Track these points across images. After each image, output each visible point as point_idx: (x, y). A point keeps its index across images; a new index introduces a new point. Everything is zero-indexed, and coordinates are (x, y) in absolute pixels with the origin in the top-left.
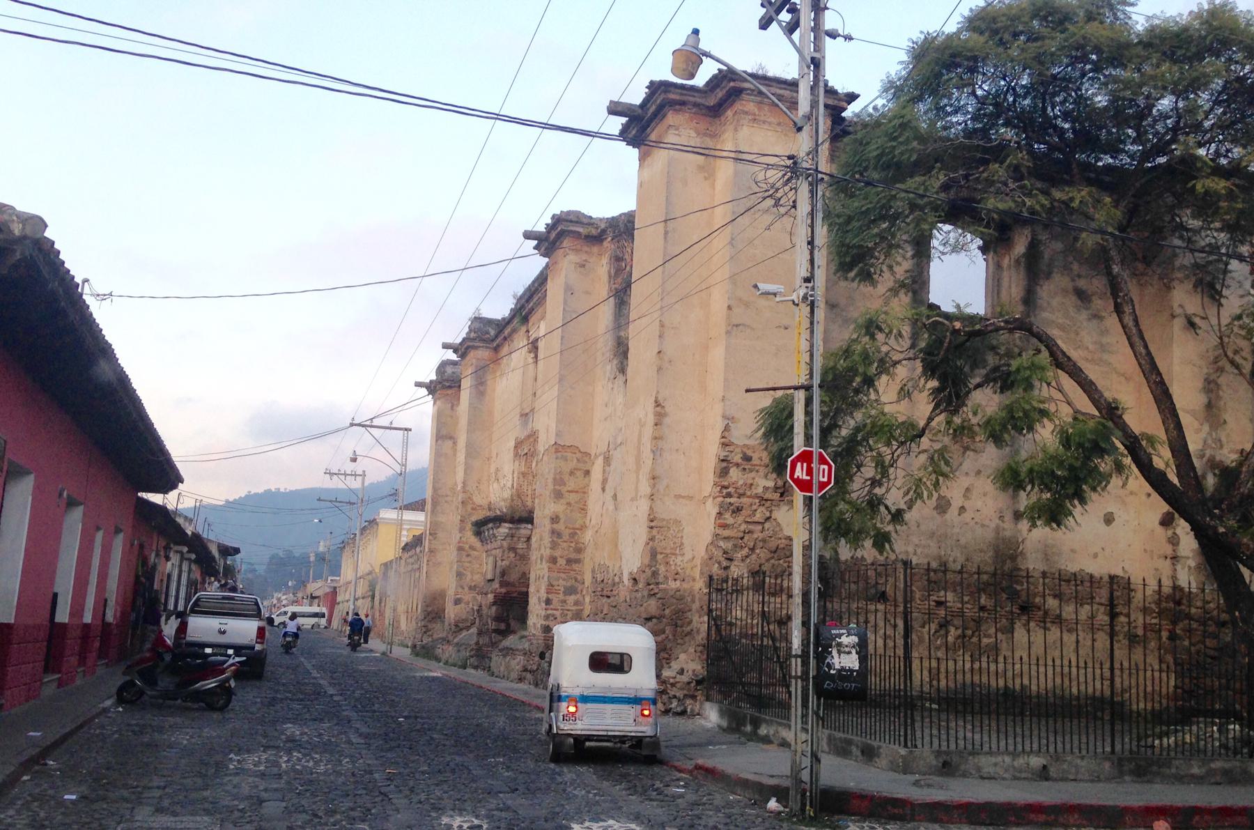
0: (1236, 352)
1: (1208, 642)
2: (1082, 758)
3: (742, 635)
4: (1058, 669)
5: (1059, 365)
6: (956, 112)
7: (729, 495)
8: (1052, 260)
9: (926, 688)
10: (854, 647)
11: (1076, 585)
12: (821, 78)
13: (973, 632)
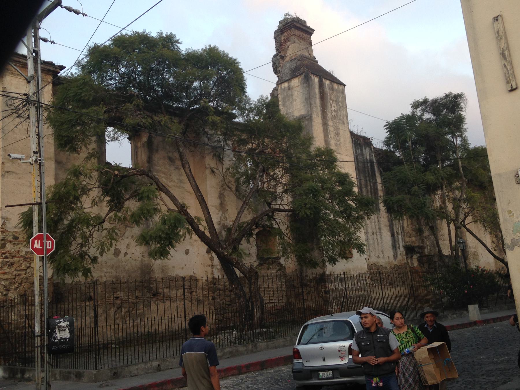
1: (227, 299)
2: (174, 358)
3: (18, 328)
5: (161, 190)
6: (111, 79)
7: (6, 257)
9: (113, 338)
10: (67, 327)
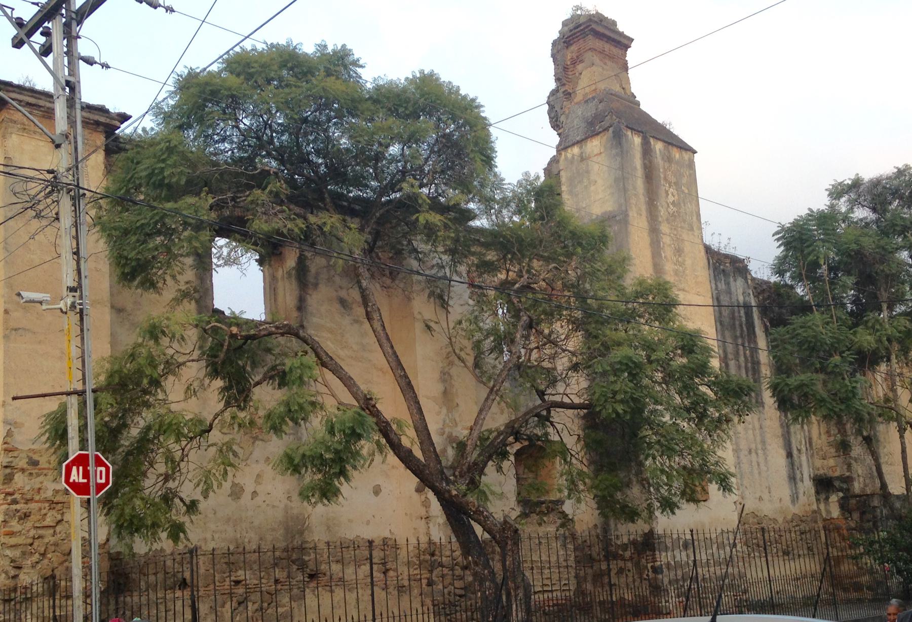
5: (324, 365)
6: (223, 140)
7: (15, 502)
8: (317, 274)
11: (355, 550)
12: (77, 101)
13: (269, 604)
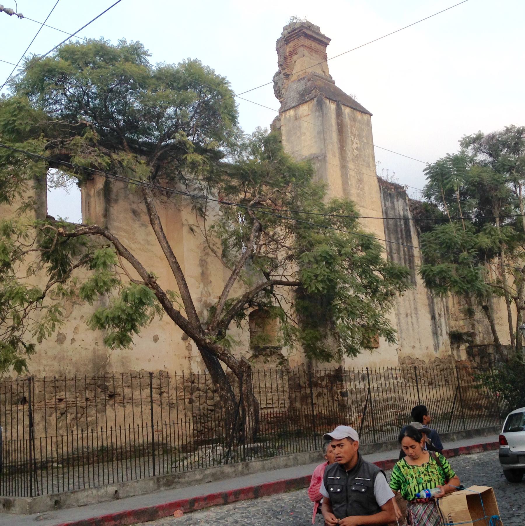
0: (214, 245)
2: (137, 482)
4: (132, 430)
5: (121, 254)
6: (56, 103)
